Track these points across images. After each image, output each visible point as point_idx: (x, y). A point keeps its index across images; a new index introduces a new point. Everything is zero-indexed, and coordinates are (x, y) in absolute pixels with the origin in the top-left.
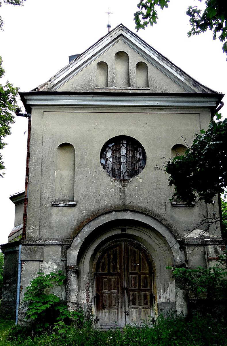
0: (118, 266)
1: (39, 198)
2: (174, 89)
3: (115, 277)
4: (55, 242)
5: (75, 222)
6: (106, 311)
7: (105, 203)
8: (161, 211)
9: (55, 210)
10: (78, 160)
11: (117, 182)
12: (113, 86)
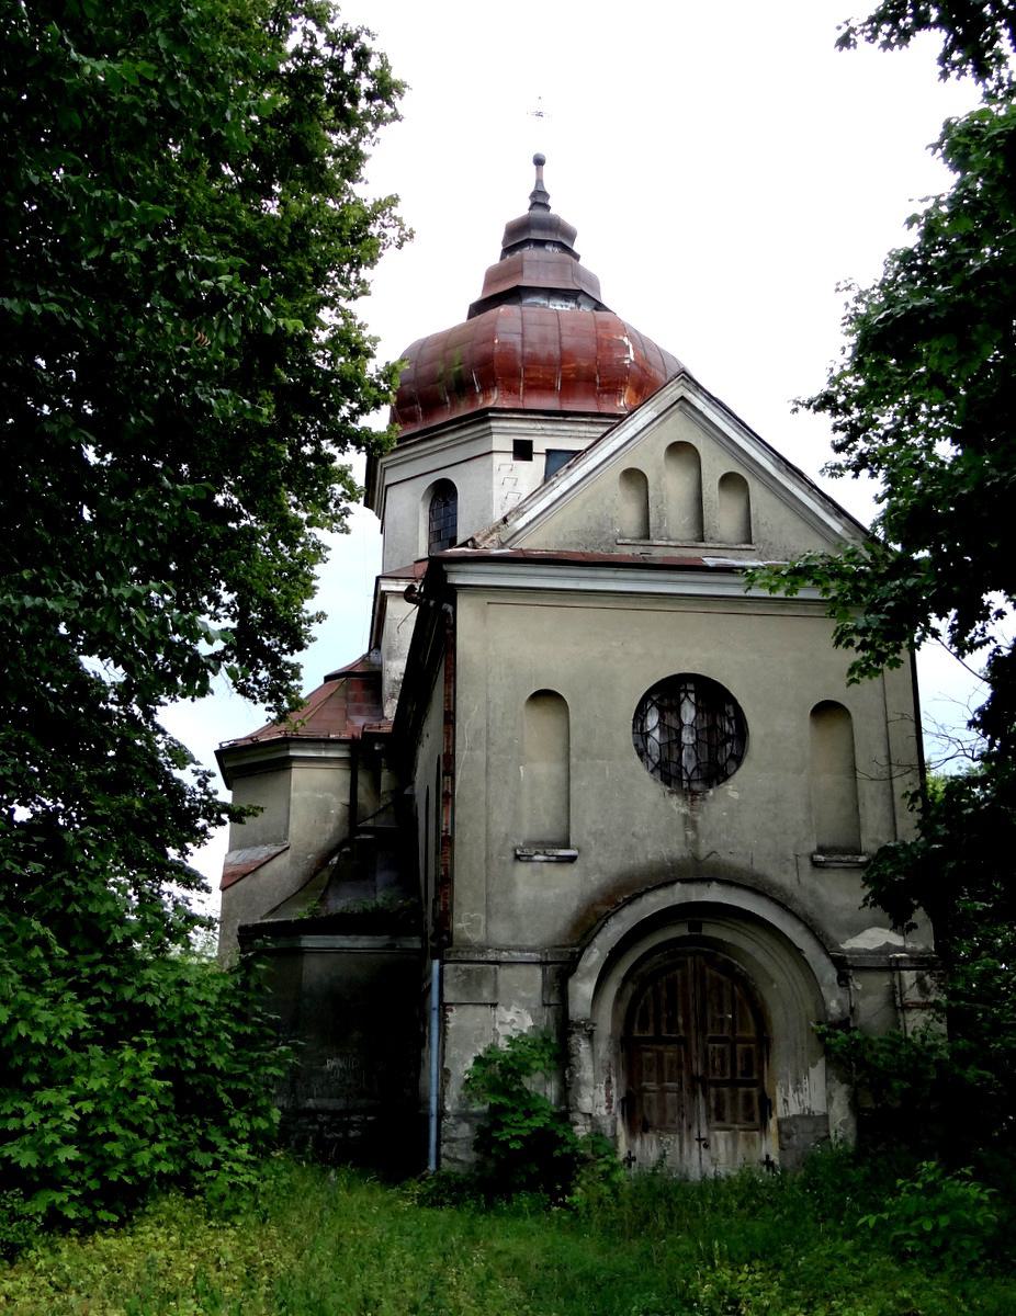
0: (680, 1020)
5: (574, 904)
6: (651, 1137)
7: (647, 853)
9: (523, 869)
11: (675, 797)
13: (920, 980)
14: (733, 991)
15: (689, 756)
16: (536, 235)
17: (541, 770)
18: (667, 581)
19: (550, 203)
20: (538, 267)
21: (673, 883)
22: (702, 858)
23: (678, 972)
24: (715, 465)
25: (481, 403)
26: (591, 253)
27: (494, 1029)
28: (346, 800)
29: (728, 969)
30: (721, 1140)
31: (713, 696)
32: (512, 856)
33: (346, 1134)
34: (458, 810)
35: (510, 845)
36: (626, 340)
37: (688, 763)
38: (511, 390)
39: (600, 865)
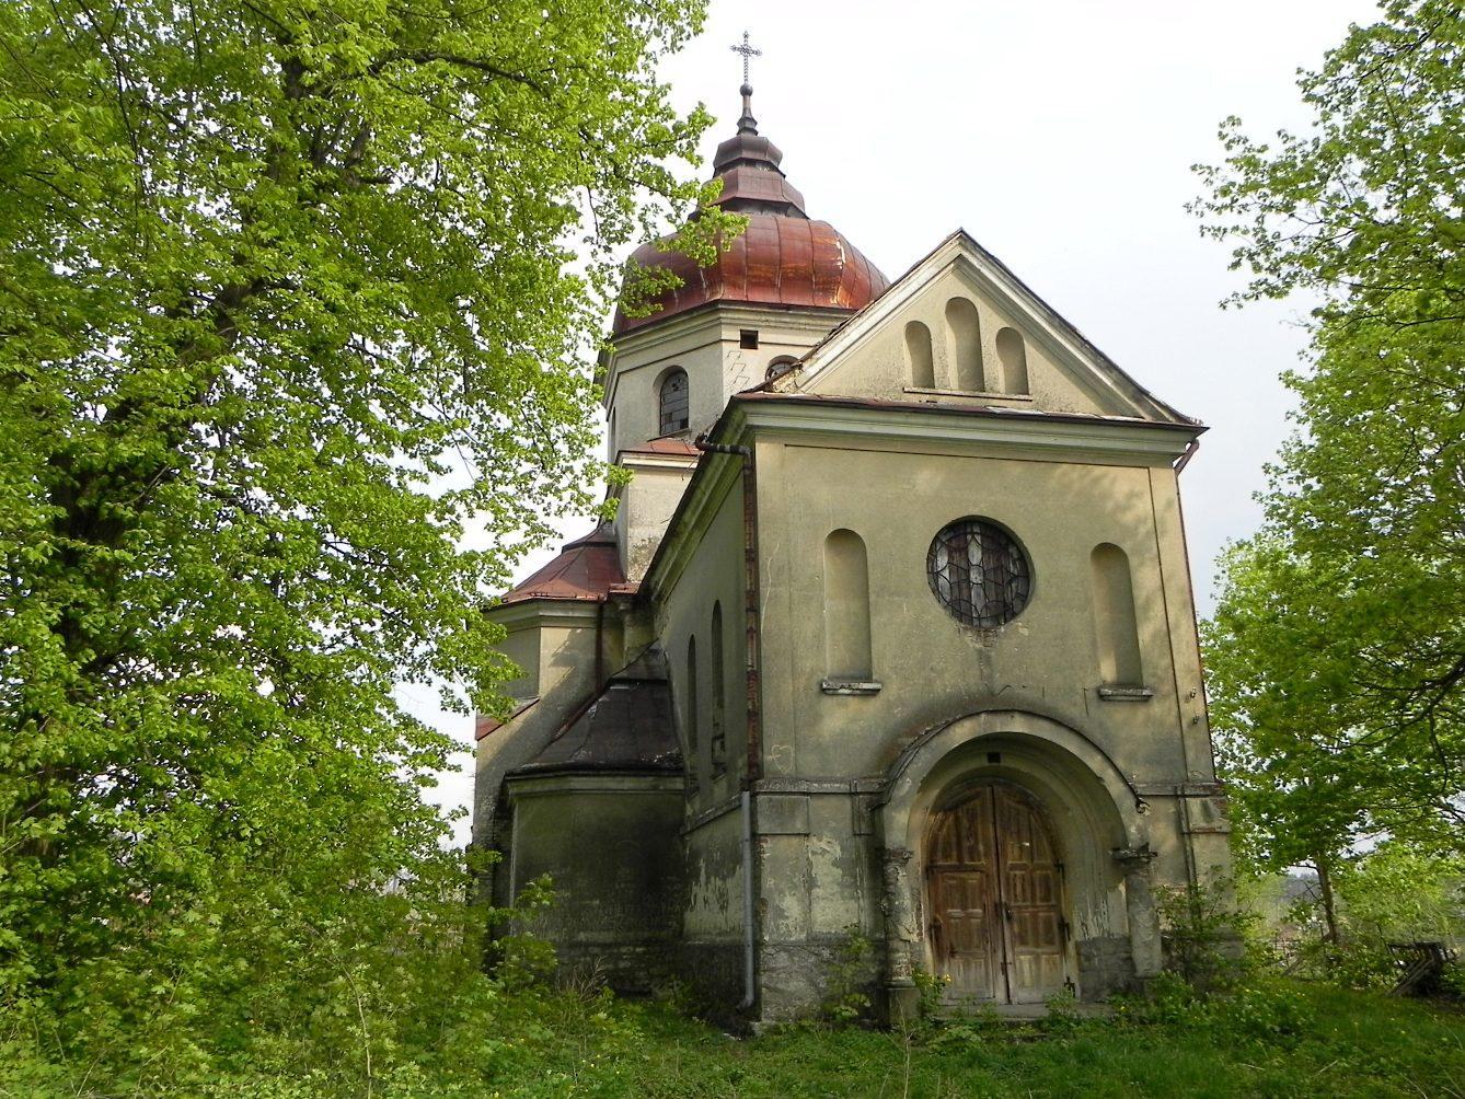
0: (981, 848)
1: (789, 670)
2: (1085, 407)
3: (977, 875)
4: (836, 787)
5: (880, 735)
6: (958, 961)
7: (946, 687)
8: (1074, 712)
9: (828, 703)
10: (875, 575)
11: (969, 634)
12: (945, 387)
13: (1205, 807)
14: (1030, 820)
15: (978, 595)
16: (746, 154)
17: (833, 606)
18: (957, 427)
19: (757, 128)
20: (751, 183)
21: (978, 714)
22: (997, 692)
23: (977, 802)
24: (991, 323)
25: (708, 298)
26: (802, 173)
27: (808, 859)
28: (592, 656)
29: (1025, 800)
30: (1024, 962)
31: (998, 537)
32: (816, 689)
33: (616, 964)
34: (764, 645)
35: (815, 679)
36: (838, 244)
37: (977, 598)
38: (734, 285)
39: (899, 694)
